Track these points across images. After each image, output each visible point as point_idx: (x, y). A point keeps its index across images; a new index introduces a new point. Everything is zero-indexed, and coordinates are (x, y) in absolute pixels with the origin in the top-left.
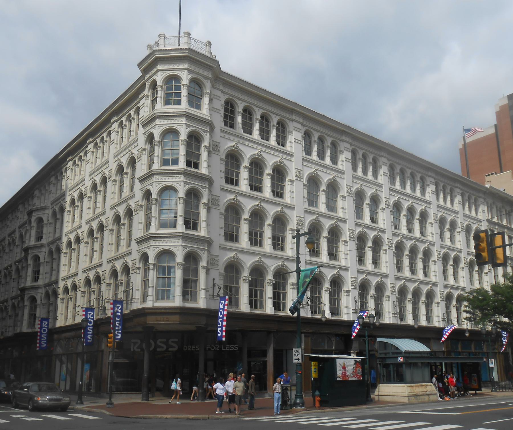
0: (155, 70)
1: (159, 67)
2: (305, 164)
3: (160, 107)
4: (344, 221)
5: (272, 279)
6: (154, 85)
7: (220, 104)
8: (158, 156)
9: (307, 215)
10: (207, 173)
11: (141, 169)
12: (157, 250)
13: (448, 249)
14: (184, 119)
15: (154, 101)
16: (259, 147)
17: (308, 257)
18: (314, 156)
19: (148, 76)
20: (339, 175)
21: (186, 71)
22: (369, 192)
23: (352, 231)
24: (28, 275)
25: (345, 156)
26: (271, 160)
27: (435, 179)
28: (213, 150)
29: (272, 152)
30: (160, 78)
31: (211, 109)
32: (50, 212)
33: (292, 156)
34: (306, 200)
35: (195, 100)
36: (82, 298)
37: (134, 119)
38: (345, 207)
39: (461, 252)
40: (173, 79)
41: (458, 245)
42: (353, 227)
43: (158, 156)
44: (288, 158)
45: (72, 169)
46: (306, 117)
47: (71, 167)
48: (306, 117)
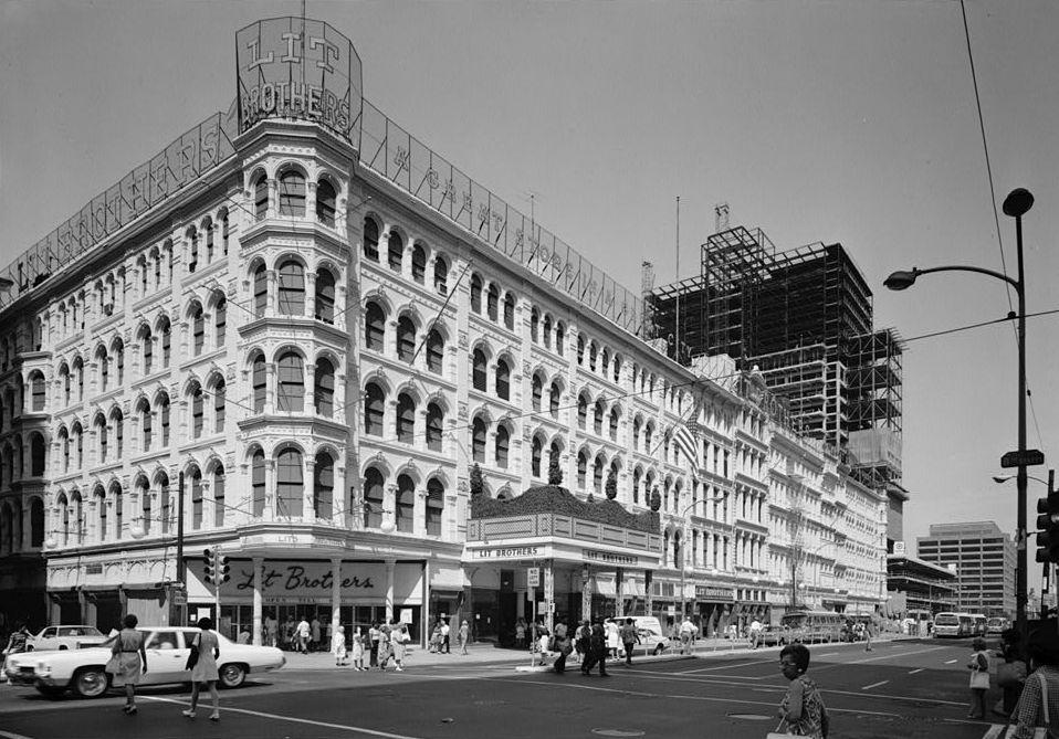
0: (263, 152)
1: (271, 148)
2: (472, 323)
3: (273, 217)
4: (566, 430)
5: (395, 484)
6: (261, 179)
7: (359, 223)
8: (273, 297)
9: (472, 401)
10: (345, 331)
11: (238, 316)
12: (277, 442)
13: (642, 459)
14: (313, 242)
15: (262, 203)
16: (382, 280)
17: (363, 434)
18: (484, 314)
19: (249, 161)
20: (515, 344)
21: (313, 161)
22: (551, 373)
23: (464, 406)
24: (25, 462)
25: (522, 316)
26: (427, 316)
27: (532, 300)
28: (352, 291)
29: (429, 303)
30: (271, 166)
31: (350, 228)
32: (56, 363)
33: (455, 311)
34: (471, 379)
35: (325, 210)
36: (133, 504)
37: (216, 226)
38: (456, 366)
39: (657, 465)
40: (291, 172)
41: (620, 442)
42: (465, 399)
43: (273, 297)
44: (450, 313)
45: (95, 296)
46: (537, 290)
47: (92, 292)
48: (537, 290)
